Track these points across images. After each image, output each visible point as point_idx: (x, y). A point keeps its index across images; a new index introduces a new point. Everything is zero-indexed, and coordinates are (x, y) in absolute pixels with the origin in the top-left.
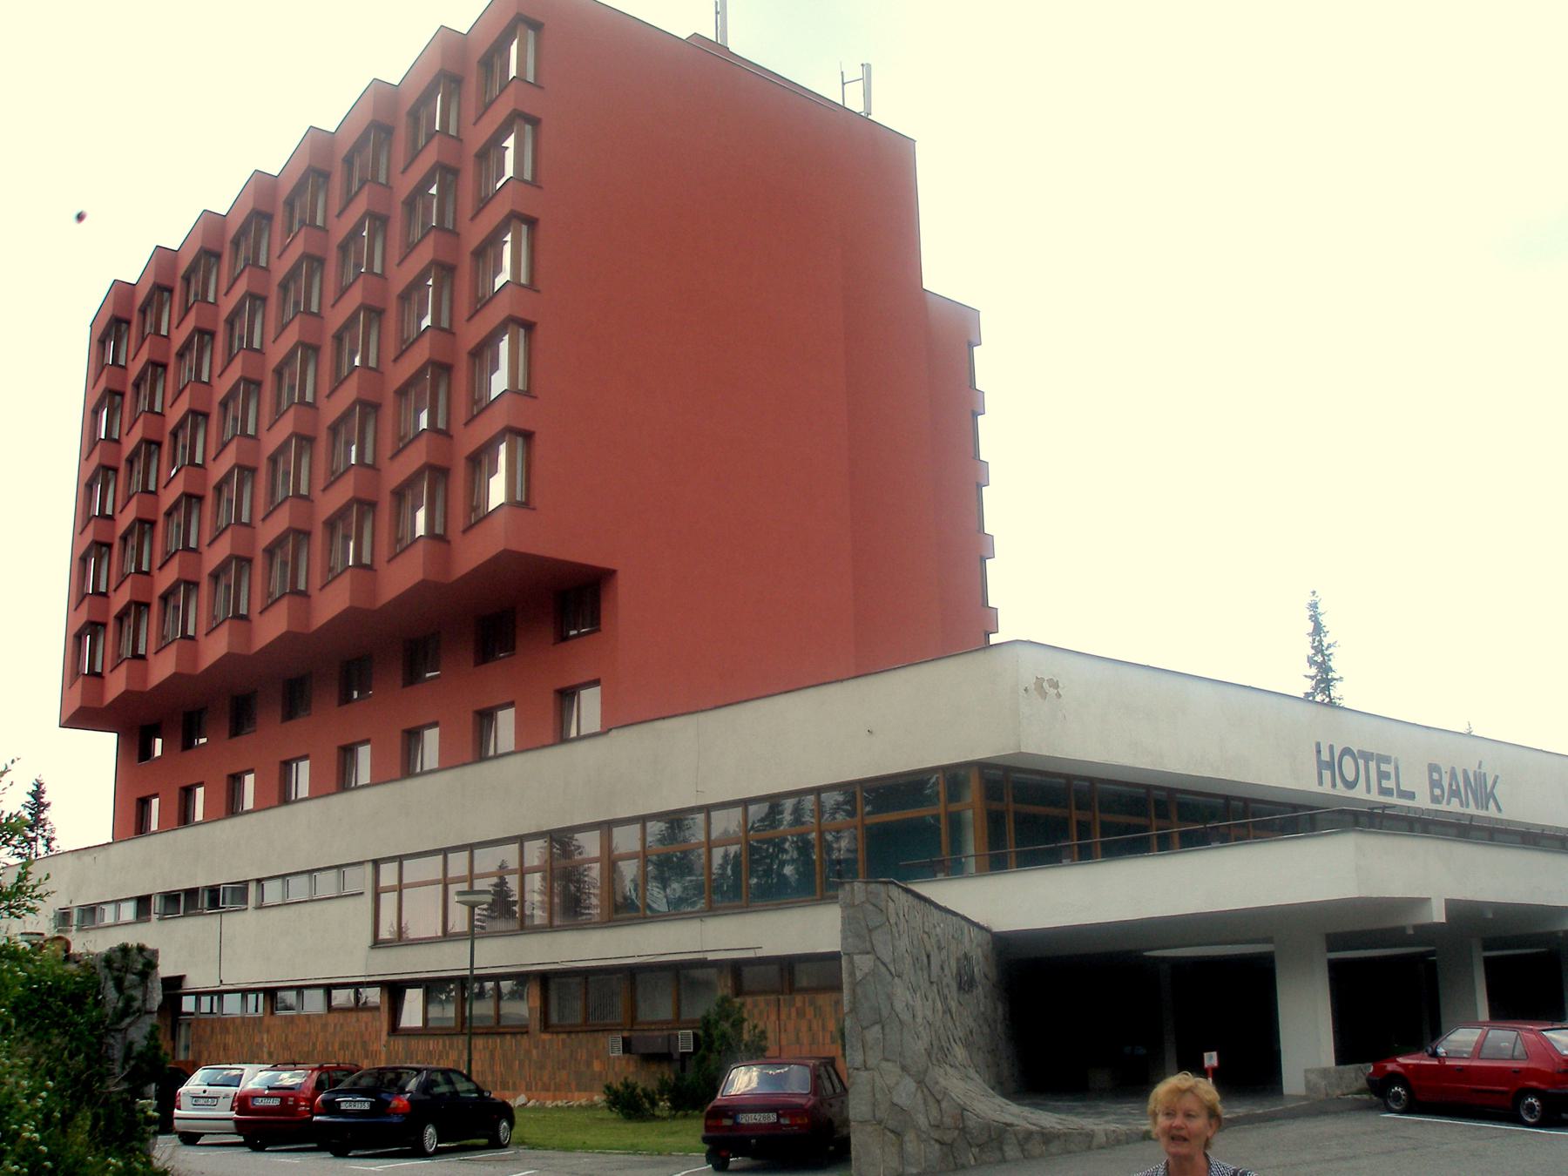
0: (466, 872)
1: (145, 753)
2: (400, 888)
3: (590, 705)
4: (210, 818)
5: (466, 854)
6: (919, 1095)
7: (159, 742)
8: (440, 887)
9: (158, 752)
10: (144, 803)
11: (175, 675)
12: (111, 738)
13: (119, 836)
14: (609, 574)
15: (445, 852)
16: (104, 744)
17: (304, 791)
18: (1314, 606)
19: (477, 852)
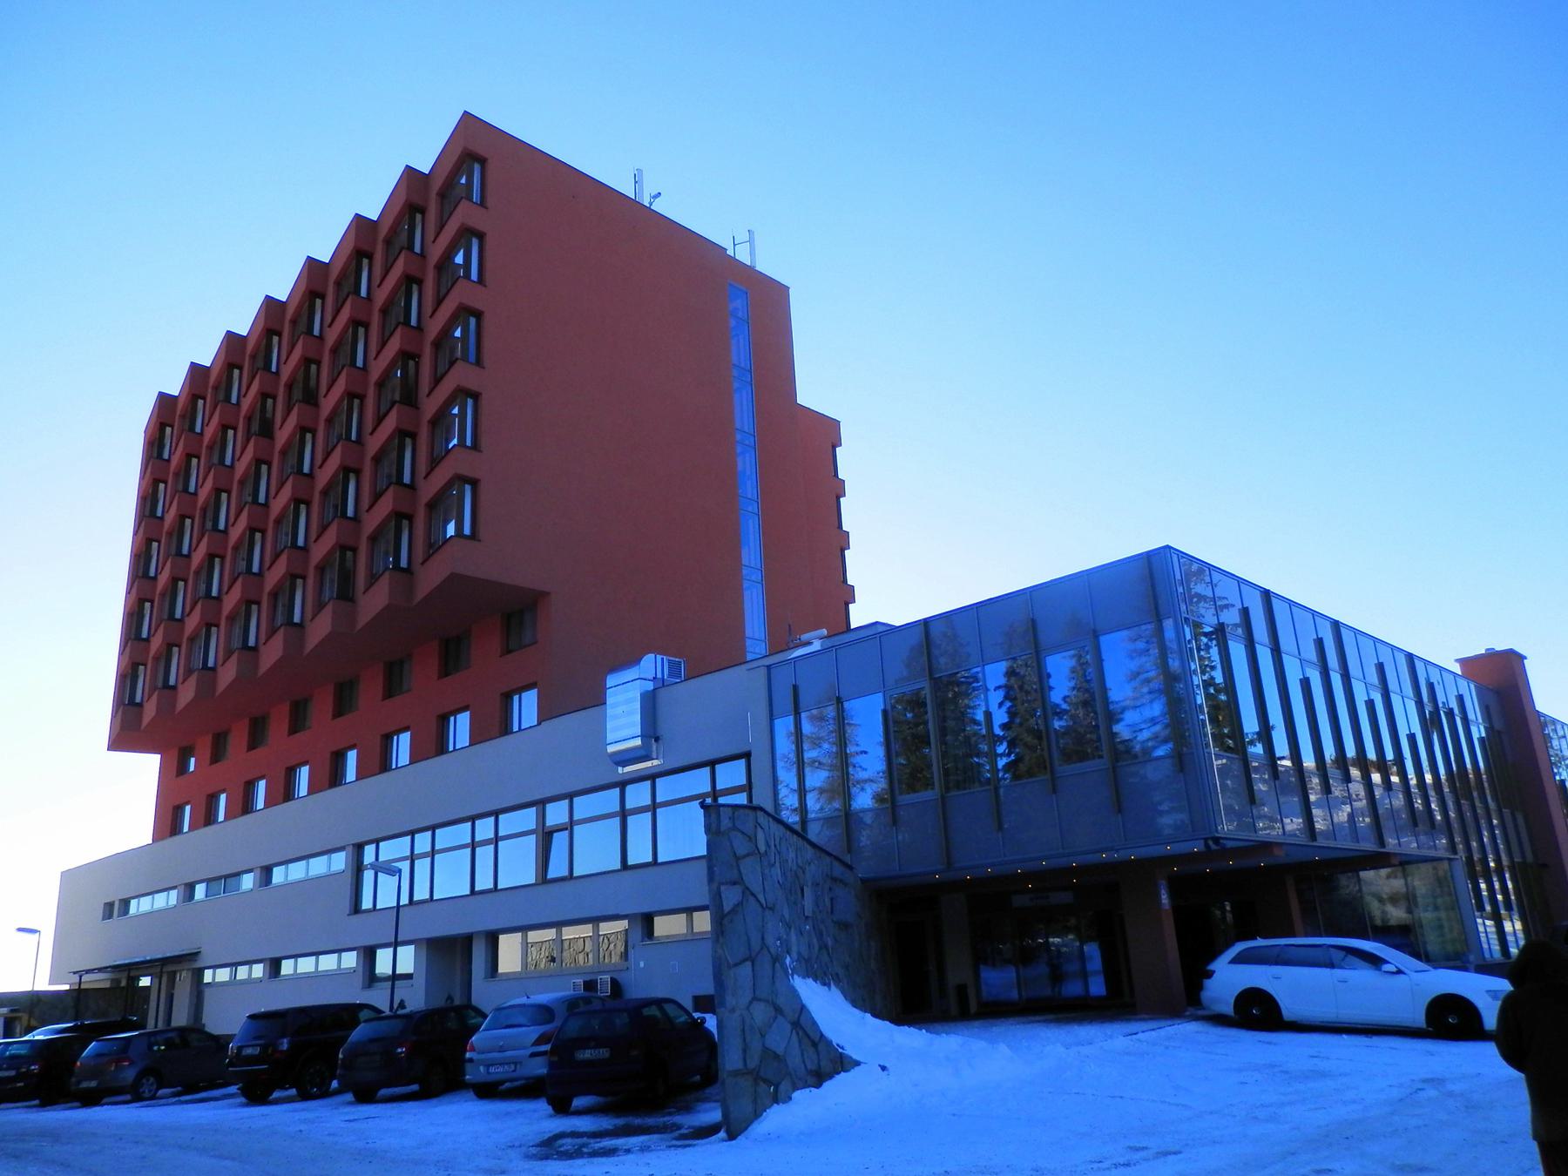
0: (429, 849)
1: (182, 768)
2: (570, 826)
3: (527, 706)
4: (269, 803)
5: (648, 783)
6: (794, 1038)
7: (193, 760)
8: (617, 820)
9: (192, 768)
10: (178, 811)
11: (387, 608)
12: (155, 759)
13: (158, 836)
14: (544, 595)
15: (712, 764)
16: (146, 768)
17: (260, 804)
18: (795, 687)
19: (438, 831)
